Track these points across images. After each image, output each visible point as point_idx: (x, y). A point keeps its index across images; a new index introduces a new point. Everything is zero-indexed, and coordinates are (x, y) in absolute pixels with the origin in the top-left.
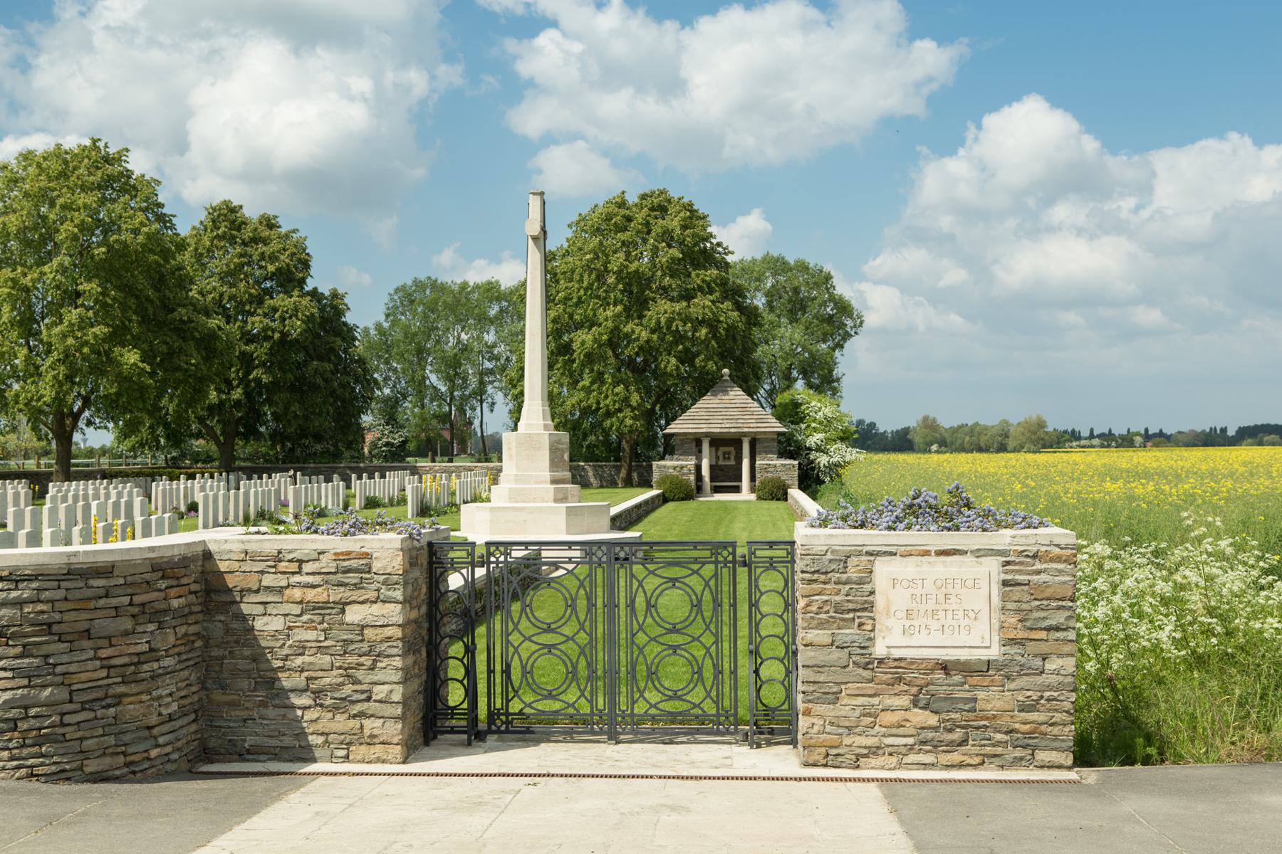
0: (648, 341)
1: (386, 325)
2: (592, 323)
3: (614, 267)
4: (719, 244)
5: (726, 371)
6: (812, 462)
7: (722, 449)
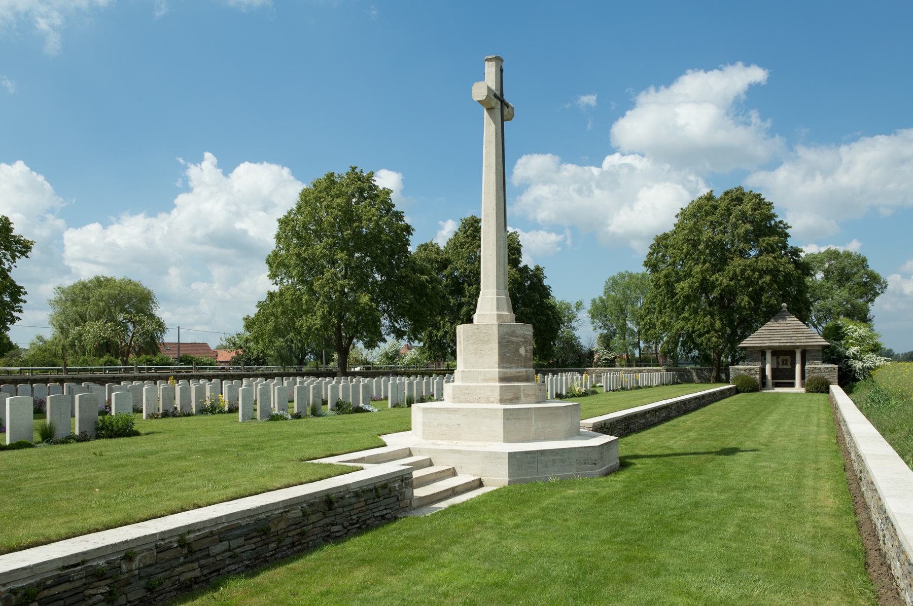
0: (728, 286)
1: (604, 298)
2: (689, 275)
3: (704, 238)
4: (781, 222)
5: (784, 304)
6: (850, 366)
7: (781, 358)
